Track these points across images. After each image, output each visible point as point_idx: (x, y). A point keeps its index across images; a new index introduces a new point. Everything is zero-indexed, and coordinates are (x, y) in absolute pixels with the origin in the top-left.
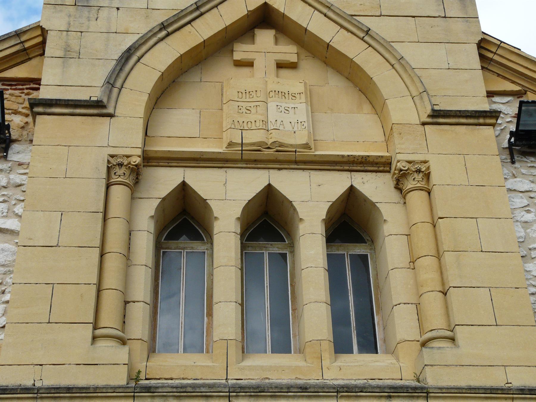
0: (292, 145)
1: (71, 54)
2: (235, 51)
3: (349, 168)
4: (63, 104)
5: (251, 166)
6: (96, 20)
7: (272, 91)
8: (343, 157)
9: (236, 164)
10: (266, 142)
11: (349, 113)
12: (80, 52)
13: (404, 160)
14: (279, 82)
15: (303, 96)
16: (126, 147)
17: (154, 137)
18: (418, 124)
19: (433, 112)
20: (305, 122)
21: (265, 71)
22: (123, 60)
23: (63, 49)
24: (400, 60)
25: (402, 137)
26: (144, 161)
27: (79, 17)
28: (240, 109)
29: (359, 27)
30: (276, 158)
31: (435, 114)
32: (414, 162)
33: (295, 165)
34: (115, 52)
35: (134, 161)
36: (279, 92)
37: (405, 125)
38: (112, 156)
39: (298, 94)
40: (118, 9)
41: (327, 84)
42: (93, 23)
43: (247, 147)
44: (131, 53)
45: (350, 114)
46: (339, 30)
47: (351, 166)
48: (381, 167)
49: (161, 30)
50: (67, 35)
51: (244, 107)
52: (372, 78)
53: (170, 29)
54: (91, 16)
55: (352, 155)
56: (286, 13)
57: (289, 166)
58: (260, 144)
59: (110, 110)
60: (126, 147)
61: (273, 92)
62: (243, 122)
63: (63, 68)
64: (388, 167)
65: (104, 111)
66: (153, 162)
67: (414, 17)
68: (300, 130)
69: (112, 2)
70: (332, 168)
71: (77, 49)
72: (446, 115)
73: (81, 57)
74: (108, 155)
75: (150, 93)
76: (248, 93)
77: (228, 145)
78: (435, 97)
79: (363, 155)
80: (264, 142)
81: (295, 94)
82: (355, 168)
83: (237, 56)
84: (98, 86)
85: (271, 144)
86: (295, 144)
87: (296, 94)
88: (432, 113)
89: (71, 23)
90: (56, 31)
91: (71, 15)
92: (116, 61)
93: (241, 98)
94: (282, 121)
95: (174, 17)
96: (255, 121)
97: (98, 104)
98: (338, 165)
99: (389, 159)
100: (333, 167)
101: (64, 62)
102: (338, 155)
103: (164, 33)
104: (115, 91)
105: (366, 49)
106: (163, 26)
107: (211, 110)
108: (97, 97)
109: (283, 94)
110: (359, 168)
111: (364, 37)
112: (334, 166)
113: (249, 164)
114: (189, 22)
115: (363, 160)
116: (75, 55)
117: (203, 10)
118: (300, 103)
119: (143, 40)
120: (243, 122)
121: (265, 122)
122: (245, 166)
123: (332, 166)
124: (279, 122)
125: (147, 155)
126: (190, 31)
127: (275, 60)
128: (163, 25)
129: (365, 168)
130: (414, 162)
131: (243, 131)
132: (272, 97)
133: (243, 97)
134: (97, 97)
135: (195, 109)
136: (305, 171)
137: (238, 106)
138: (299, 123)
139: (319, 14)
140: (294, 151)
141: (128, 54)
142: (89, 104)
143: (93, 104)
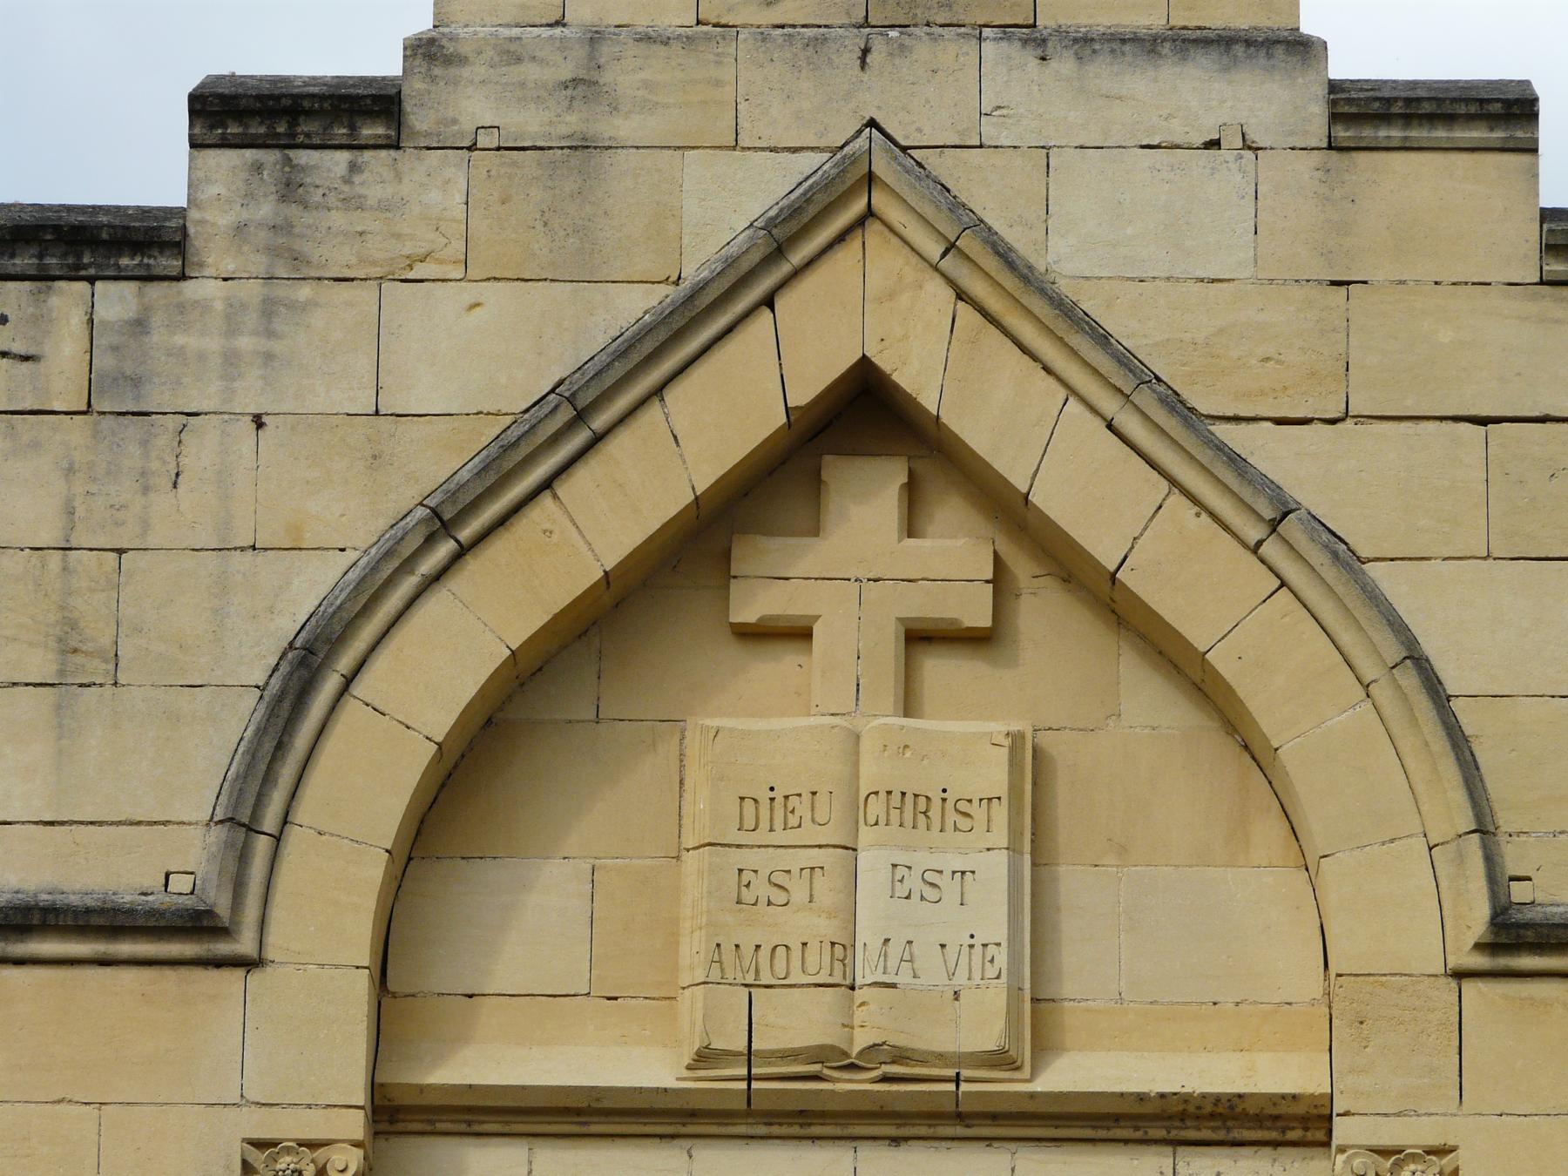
0: (941, 1058)
1: (83, 666)
2: (735, 577)
3: (1169, 1132)
4: (72, 925)
5: (784, 1130)
6: (175, 485)
7: (876, 793)
8: (1141, 1099)
9: (727, 1124)
10: (842, 1046)
11: (1191, 866)
12: (116, 655)
13: (1360, 1147)
14: (906, 747)
15: (1001, 813)
16: (309, 1106)
17: (413, 996)
18: (1436, 976)
19: (1496, 934)
20: (998, 944)
21: (858, 679)
22: (286, 705)
23: (53, 644)
24: (1394, 671)
25: (1365, 1039)
26: (376, 1118)
27: (108, 473)
28: (748, 885)
29: (1241, 500)
30: (882, 1107)
31: (1503, 940)
32: (1400, 1152)
33: (955, 1125)
34: (252, 647)
35: (340, 1169)
36: (903, 794)
37: (1384, 978)
38: (260, 1145)
39: (981, 800)
40: (258, 422)
41: (1113, 717)
42: (162, 501)
43: (770, 1064)
44: (336, 132)
45: (1195, 869)
46: (1164, 500)
47: (1176, 1128)
48: (1293, 1128)
49: (430, 540)
50: (64, 569)
51: (763, 873)
52: (1276, 750)
53: (466, 533)
54: (155, 465)
55: (1175, 1094)
56: (944, 419)
57: (932, 1130)
58: (820, 1054)
59: (245, 945)
60: (309, 1106)
61: (883, 795)
62: (758, 947)
63: (60, 739)
64: (1318, 1129)
65: (223, 948)
66: (410, 1121)
67: (1483, 421)
68: (978, 987)
69: (236, 384)
70: (1102, 1134)
71: (106, 640)
72: (1547, 943)
73: (122, 679)
74: (244, 1140)
75: (393, 845)
76: (779, 801)
77: (696, 1058)
78: (1523, 838)
79: (1219, 1093)
80: (833, 1048)
81: (970, 801)
82: (1192, 1134)
83: (751, 606)
84: (193, 819)
85: (861, 1053)
86: (955, 1052)
87: (976, 802)
88: (1493, 936)
89: (76, 504)
90: (22, 550)
91: (77, 466)
92: (258, 692)
93: (753, 830)
94: (910, 942)
95: (483, 473)
96: (805, 944)
97: (198, 924)
98: (1122, 1124)
99: (1322, 1105)
100: (1105, 1132)
101: (58, 708)
102: (1122, 1094)
103: (445, 549)
104: (262, 845)
105: (1264, 601)
106: (440, 523)
107: (636, 862)
108: (192, 873)
109: (922, 801)
110: (1206, 1134)
111: (1260, 543)
112: (1108, 1129)
113: (780, 1124)
114: (547, 485)
115: (1220, 1110)
116: (97, 670)
117: (600, 422)
118: (988, 849)
119: (363, 600)
120: (758, 947)
121: (844, 949)
122: (762, 1130)
123: (1102, 1128)
124: (895, 950)
125: (389, 1100)
126: (548, 526)
127: (899, 620)
128: (441, 519)
129: (1228, 1132)
130: (1400, 1152)
131: (983, 112)
132: (876, 824)
133: (761, 826)
134: (192, 873)
135: (574, 858)
136: (996, 1144)
137: (740, 871)
138: (978, 949)
139: (1088, 415)
140: (950, 1077)
141: (305, 673)
142: (163, 923)
143: (179, 923)
